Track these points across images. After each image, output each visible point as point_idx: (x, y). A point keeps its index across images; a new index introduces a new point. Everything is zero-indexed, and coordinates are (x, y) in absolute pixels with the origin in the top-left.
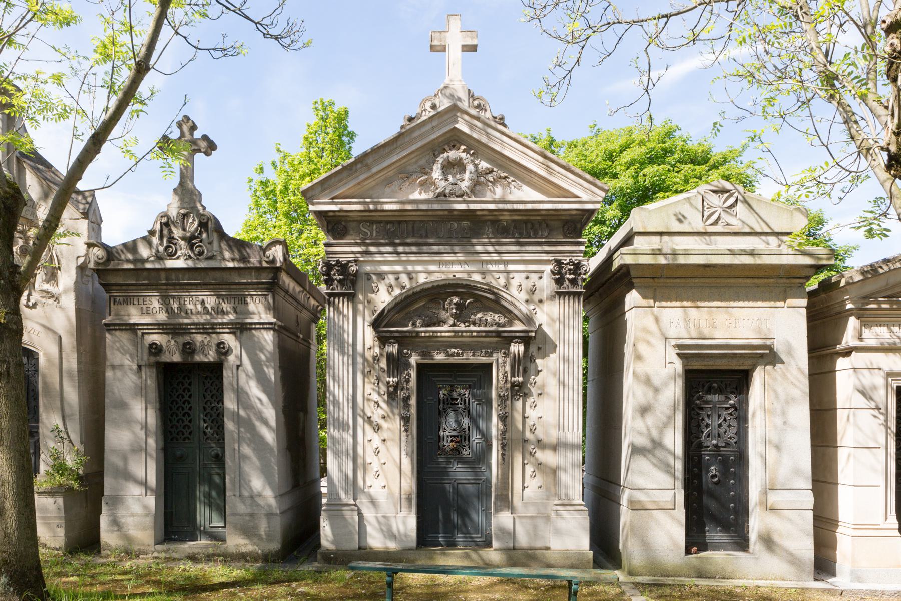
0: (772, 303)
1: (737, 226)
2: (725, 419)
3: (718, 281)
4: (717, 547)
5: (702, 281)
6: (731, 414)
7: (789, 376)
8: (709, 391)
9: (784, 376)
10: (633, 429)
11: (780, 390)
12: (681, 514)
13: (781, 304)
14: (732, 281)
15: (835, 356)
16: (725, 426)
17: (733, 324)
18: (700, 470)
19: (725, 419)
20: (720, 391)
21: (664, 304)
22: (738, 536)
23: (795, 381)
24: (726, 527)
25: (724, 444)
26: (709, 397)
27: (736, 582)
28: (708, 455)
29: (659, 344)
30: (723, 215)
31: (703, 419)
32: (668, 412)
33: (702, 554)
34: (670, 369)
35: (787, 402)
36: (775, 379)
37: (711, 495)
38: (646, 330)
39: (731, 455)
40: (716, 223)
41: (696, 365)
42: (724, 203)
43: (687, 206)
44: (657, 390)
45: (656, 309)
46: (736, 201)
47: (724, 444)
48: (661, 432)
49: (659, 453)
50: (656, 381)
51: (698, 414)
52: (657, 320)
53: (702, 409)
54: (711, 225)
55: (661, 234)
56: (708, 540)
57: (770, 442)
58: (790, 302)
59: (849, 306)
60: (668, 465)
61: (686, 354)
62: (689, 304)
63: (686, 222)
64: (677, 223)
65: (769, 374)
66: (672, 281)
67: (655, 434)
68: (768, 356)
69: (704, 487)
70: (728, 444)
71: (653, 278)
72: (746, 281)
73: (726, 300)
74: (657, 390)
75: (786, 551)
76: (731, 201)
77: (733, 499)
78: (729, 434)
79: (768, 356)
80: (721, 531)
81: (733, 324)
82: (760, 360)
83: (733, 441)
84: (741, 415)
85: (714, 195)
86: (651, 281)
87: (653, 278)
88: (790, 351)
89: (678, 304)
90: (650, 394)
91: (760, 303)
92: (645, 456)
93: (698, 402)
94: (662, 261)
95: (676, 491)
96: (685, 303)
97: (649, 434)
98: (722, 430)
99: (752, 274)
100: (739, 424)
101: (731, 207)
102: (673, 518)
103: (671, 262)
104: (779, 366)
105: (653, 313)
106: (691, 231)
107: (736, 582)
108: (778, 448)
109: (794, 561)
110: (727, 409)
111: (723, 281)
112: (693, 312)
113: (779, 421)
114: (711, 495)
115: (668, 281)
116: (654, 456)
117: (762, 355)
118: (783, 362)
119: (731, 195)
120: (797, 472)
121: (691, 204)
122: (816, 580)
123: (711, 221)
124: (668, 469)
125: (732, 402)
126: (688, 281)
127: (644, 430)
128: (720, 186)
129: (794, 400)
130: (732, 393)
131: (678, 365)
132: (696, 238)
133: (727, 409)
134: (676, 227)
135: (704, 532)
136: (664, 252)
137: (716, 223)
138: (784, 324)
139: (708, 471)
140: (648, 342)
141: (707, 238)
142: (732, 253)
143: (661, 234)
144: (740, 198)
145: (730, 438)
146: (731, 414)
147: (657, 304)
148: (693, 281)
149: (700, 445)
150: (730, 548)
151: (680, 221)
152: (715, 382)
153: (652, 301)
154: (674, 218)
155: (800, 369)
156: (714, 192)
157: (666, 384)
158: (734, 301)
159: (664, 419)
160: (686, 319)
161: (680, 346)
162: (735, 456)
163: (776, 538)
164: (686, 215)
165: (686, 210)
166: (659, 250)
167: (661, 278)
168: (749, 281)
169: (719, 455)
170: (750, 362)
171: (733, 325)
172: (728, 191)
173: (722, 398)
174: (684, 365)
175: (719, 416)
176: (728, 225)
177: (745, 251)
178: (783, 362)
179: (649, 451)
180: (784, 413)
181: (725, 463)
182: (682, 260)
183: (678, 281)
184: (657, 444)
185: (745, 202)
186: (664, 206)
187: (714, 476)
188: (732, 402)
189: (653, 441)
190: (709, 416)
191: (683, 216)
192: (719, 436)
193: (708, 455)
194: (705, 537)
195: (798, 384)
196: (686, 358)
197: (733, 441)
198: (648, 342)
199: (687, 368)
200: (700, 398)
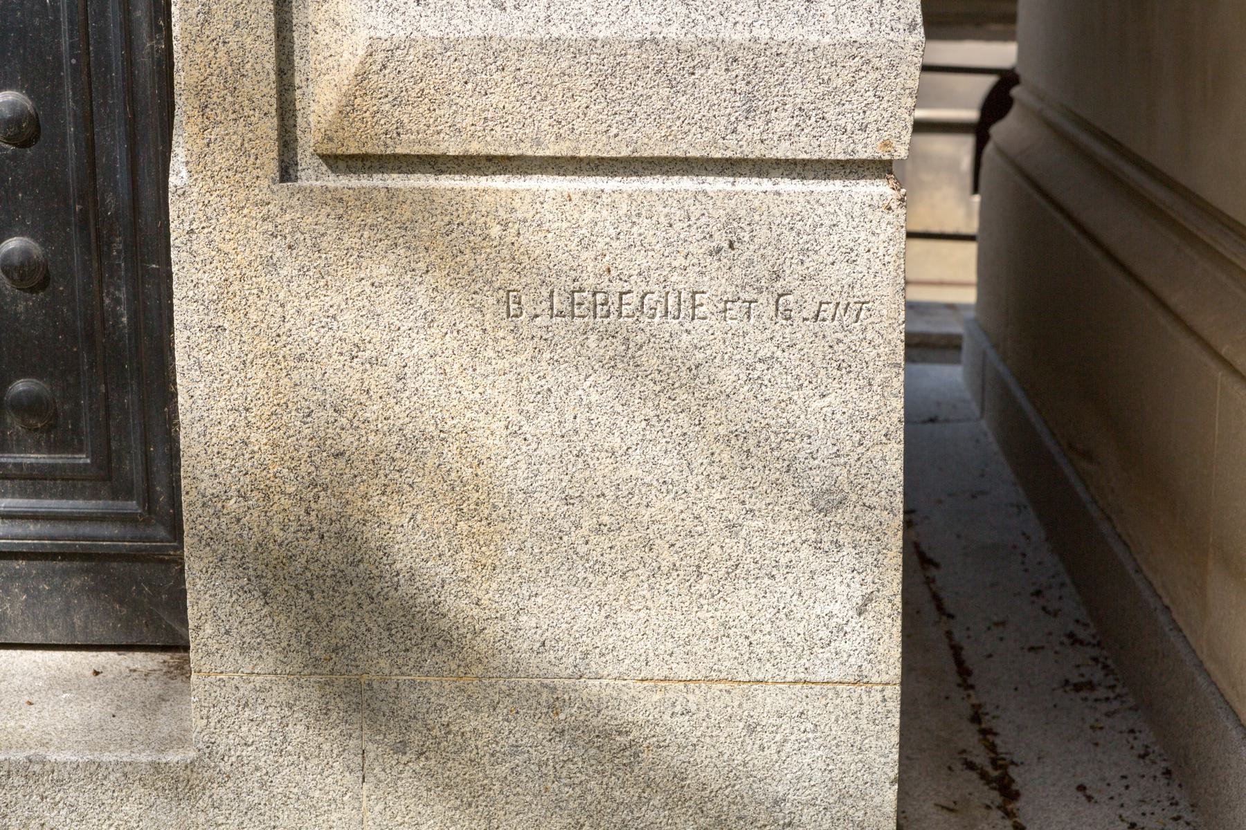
163: (415, 540)
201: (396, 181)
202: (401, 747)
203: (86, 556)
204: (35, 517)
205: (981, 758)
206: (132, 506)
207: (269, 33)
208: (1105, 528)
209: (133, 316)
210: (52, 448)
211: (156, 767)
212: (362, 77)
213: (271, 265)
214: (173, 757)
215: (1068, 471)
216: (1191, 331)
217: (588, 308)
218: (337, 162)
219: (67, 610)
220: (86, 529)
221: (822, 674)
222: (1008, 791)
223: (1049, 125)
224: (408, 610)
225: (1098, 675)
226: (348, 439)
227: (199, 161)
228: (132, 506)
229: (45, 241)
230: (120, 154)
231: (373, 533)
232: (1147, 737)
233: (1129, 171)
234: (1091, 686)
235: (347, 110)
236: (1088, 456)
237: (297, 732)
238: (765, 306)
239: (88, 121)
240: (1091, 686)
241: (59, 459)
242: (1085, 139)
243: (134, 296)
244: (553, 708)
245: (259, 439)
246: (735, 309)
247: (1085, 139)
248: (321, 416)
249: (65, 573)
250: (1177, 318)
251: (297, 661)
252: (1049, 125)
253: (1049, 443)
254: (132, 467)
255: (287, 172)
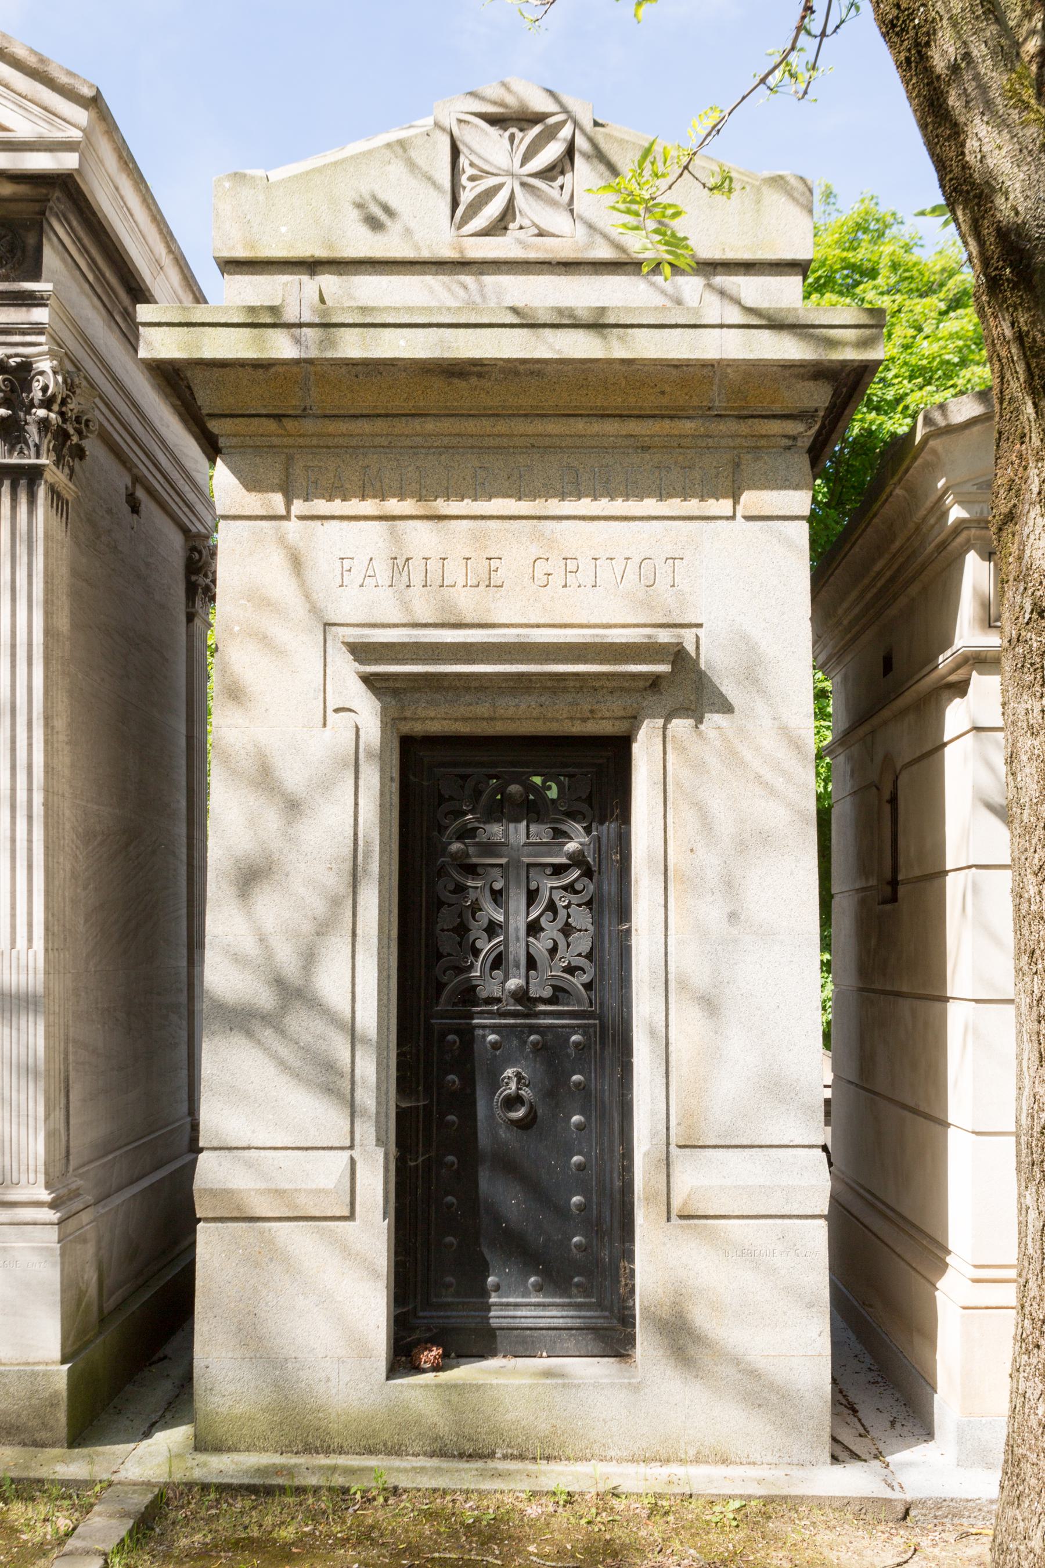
0: (693, 506)
1: (569, 240)
2: (552, 907)
3: (502, 427)
4: (524, 1343)
5: (446, 425)
6: (570, 888)
7: (748, 755)
8: (497, 812)
9: (733, 759)
10: (235, 946)
11: (717, 805)
12: (372, 1236)
13: (724, 506)
14: (553, 427)
15: (945, 695)
16: (551, 931)
17: (554, 573)
18: (469, 1081)
19: (552, 907)
20: (533, 809)
21: (321, 506)
22: (600, 1306)
23: (768, 776)
24: (555, 1273)
25: (547, 992)
26: (495, 831)
27: (559, 1476)
28: (494, 1029)
29: (303, 647)
30: (522, 200)
31: (476, 908)
32: (336, 882)
33: (466, 1372)
34: (338, 735)
35: (742, 847)
36: (699, 767)
37: (507, 1165)
38: (264, 602)
39: (574, 1029)
40: (500, 226)
41: (436, 720)
42: (525, 161)
43: (397, 169)
44: (293, 807)
45: (292, 526)
46: (570, 152)
47: (547, 992)
48: (309, 958)
49: (302, 1024)
50: (294, 776)
51: (461, 889)
52: (296, 563)
53: (472, 870)
54: (486, 233)
55: (312, 266)
56: (497, 1317)
57: (683, 985)
58: (753, 500)
59: (956, 513)
60: (329, 1067)
61: (395, 677)
62: (408, 506)
63: (394, 228)
64: (364, 231)
65: (682, 749)
66: (343, 426)
67: (287, 958)
68: (677, 682)
69: (484, 1140)
70: (559, 993)
71: (278, 417)
72: (597, 427)
73: (533, 496)
74: (293, 807)
75: (736, 1361)
76: (553, 151)
77: (581, 1178)
78: (567, 956)
79: (677, 682)
80: (539, 1289)
81: (554, 573)
82: (650, 700)
83: (577, 981)
84: (605, 887)
85: (493, 131)
86: (272, 426)
87: (278, 417)
88: (752, 675)
89: (369, 506)
90: (272, 819)
91: (650, 506)
92: (249, 1034)
93: (455, 846)
94: (282, 347)
95: (356, 1153)
96: (393, 506)
97: (269, 955)
98: (541, 945)
99: (616, 401)
100: (598, 923)
101: (549, 173)
102: (346, 1251)
103: (313, 353)
104: (713, 720)
105: (282, 540)
106: (409, 254)
107: (559, 1476)
108: (709, 1005)
109: (759, 1391)
110: (558, 870)
111: (521, 426)
112: (421, 537)
113: (712, 912)
114: (507, 1165)
115: (332, 427)
116: (281, 1031)
117: (655, 682)
118: (727, 708)
119: (550, 134)
120: (776, 1088)
121: (412, 165)
122: (841, 1453)
123: (480, 222)
124: (332, 1082)
125: (571, 846)
126: (401, 426)
127: (249, 945)
128: (511, 100)
129: (765, 838)
130: (572, 815)
131: (368, 715)
132: (429, 279)
133: (558, 870)
134: (361, 243)
135: (485, 1293)
136: (290, 315)
137: (500, 226)
138: (740, 576)
139: (495, 1084)
140: (265, 641)
141: (468, 280)
142: (527, 322)
143: (312, 266)
144: (581, 142)
145: (571, 970)
146: (570, 888)
147: (299, 506)
148: (416, 424)
149: (469, 995)
150: (570, 1345)
151: (374, 224)
152: (507, 783)
153: (277, 501)
154: (355, 214)
155: (785, 732)
156: (494, 120)
157: (325, 785)
158: (563, 496)
159: (319, 906)
160: (399, 564)
161: (360, 651)
162: (585, 1030)
163: (700, 1317)
164: (393, 204)
165: (395, 186)
166: (273, 310)
167: (303, 414)
168: (611, 427)
169: (533, 1029)
170: (615, 706)
171: (557, 580)
172: (538, 118)
173: (541, 832)
174: (389, 721)
175: (532, 896)
176: (541, 234)
177: (570, 312)
178: (727, 708)
179: (267, 1019)
180: (729, 885)
181: (550, 1052)
182: (352, 346)
183: (366, 426)
184: (294, 993)
185: (599, 156)
186: (319, 170)
187: (513, 1102)
188: (571, 846)
189: (280, 983)
190: (497, 896)
191: (387, 210)
192: (531, 963)
193: (494, 1029)
194: (488, 1308)
195: (779, 783)
196: (396, 692)
197: (577, 981)
198: (265, 641)
199: (406, 728)
200: (466, 833)
201: (696, 1221)
202: (696, 1376)
203: (593, 1329)
204: (579, 1317)
205: (844, 1402)
206: (607, 1314)
207: (665, 1185)
208: (879, 1330)
209: (610, 1259)
210: (585, 1297)
211: (630, 1384)
212: (689, 1195)
213: (664, 1244)
214: (633, 1381)
215: (863, 1312)
216: (903, 1259)
217: (747, 1253)
218: (682, 1217)
219: (587, 1345)
220: (594, 1321)
221: (810, 1353)
222: (855, 1411)
223: (847, 1184)
224: (699, 1338)
225: (880, 1379)
226: (684, 1290)
227: (646, 1217)
228: (607, 1314)
229: (586, 1237)
230: (608, 1213)
231: (689, 1316)
232: (898, 1395)
233: (879, 1204)
234: (877, 1382)
235: (685, 1204)
236: (871, 1306)
237: (668, 1373)
238: (792, 1253)
239: (599, 1204)
240: (877, 1382)
241: (587, 1300)
242: (862, 1191)
243: (610, 1252)
244: (738, 1364)
245: (660, 1291)
246: (784, 1254)
247: (862, 1191)
248: (676, 1284)
249: (587, 1334)
250: (899, 1256)
251: (669, 1352)
252: (847, 1184)
253: (856, 1303)
254: (607, 1303)
255: (669, 1220)
